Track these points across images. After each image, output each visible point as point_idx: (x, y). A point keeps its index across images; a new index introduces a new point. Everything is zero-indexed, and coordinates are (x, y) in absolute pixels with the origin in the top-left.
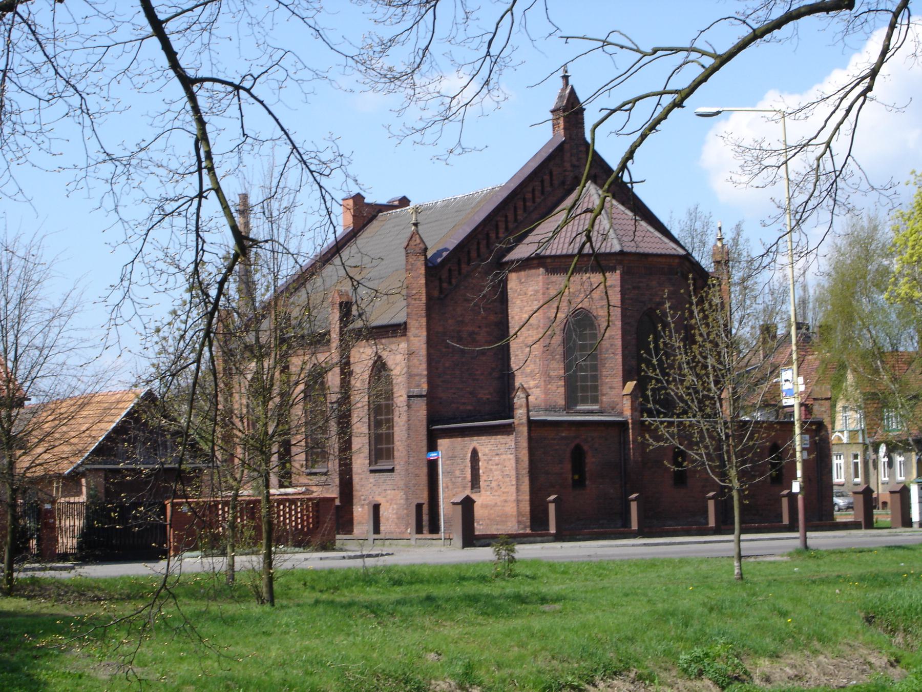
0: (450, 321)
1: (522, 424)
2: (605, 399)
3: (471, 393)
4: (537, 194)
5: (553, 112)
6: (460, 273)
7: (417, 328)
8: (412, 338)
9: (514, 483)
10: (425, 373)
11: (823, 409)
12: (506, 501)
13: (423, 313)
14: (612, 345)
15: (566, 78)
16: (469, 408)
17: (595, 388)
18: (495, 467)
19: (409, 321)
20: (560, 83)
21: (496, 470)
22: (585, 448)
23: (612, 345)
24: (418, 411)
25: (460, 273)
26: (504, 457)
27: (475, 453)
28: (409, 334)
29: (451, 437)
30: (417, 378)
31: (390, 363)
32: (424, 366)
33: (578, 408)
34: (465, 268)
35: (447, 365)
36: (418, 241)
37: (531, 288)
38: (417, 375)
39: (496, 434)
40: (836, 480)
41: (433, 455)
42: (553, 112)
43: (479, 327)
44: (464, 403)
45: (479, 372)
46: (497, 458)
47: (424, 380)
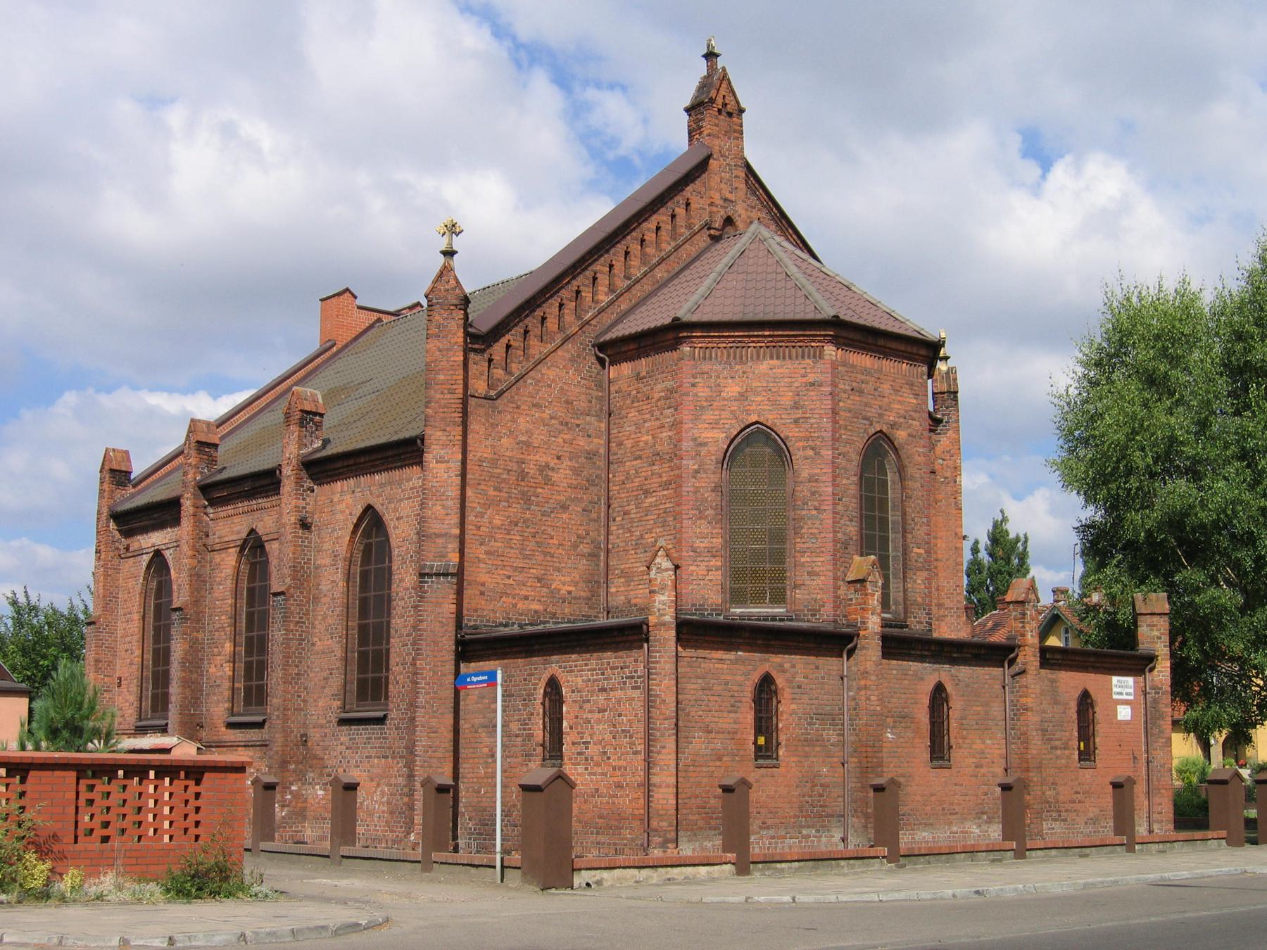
0: (505, 440)
1: (664, 624)
2: (799, 594)
3: (539, 580)
5: (688, 110)
7: (444, 446)
8: (433, 465)
9: (640, 748)
11: (1156, 633)
12: (619, 786)
14: (813, 493)
15: (711, 56)
16: (535, 606)
17: (780, 576)
18: (596, 715)
19: (428, 431)
20: (702, 68)
21: (599, 721)
22: (780, 681)
23: (813, 493)
24: (439, 604)
26: (619, 694)
27: (553, 687)
28: (428, 457)
30: (440, 541)
31: (389, 518)
35: (497, 522)
36: (452, 282)
37: (659, 386)
39: (602, 648)
40: (1115, 679)
41: (870, 650)
42: (688, 110)
43: (559, 458)
44: (526, 598)
46: (602, 697)
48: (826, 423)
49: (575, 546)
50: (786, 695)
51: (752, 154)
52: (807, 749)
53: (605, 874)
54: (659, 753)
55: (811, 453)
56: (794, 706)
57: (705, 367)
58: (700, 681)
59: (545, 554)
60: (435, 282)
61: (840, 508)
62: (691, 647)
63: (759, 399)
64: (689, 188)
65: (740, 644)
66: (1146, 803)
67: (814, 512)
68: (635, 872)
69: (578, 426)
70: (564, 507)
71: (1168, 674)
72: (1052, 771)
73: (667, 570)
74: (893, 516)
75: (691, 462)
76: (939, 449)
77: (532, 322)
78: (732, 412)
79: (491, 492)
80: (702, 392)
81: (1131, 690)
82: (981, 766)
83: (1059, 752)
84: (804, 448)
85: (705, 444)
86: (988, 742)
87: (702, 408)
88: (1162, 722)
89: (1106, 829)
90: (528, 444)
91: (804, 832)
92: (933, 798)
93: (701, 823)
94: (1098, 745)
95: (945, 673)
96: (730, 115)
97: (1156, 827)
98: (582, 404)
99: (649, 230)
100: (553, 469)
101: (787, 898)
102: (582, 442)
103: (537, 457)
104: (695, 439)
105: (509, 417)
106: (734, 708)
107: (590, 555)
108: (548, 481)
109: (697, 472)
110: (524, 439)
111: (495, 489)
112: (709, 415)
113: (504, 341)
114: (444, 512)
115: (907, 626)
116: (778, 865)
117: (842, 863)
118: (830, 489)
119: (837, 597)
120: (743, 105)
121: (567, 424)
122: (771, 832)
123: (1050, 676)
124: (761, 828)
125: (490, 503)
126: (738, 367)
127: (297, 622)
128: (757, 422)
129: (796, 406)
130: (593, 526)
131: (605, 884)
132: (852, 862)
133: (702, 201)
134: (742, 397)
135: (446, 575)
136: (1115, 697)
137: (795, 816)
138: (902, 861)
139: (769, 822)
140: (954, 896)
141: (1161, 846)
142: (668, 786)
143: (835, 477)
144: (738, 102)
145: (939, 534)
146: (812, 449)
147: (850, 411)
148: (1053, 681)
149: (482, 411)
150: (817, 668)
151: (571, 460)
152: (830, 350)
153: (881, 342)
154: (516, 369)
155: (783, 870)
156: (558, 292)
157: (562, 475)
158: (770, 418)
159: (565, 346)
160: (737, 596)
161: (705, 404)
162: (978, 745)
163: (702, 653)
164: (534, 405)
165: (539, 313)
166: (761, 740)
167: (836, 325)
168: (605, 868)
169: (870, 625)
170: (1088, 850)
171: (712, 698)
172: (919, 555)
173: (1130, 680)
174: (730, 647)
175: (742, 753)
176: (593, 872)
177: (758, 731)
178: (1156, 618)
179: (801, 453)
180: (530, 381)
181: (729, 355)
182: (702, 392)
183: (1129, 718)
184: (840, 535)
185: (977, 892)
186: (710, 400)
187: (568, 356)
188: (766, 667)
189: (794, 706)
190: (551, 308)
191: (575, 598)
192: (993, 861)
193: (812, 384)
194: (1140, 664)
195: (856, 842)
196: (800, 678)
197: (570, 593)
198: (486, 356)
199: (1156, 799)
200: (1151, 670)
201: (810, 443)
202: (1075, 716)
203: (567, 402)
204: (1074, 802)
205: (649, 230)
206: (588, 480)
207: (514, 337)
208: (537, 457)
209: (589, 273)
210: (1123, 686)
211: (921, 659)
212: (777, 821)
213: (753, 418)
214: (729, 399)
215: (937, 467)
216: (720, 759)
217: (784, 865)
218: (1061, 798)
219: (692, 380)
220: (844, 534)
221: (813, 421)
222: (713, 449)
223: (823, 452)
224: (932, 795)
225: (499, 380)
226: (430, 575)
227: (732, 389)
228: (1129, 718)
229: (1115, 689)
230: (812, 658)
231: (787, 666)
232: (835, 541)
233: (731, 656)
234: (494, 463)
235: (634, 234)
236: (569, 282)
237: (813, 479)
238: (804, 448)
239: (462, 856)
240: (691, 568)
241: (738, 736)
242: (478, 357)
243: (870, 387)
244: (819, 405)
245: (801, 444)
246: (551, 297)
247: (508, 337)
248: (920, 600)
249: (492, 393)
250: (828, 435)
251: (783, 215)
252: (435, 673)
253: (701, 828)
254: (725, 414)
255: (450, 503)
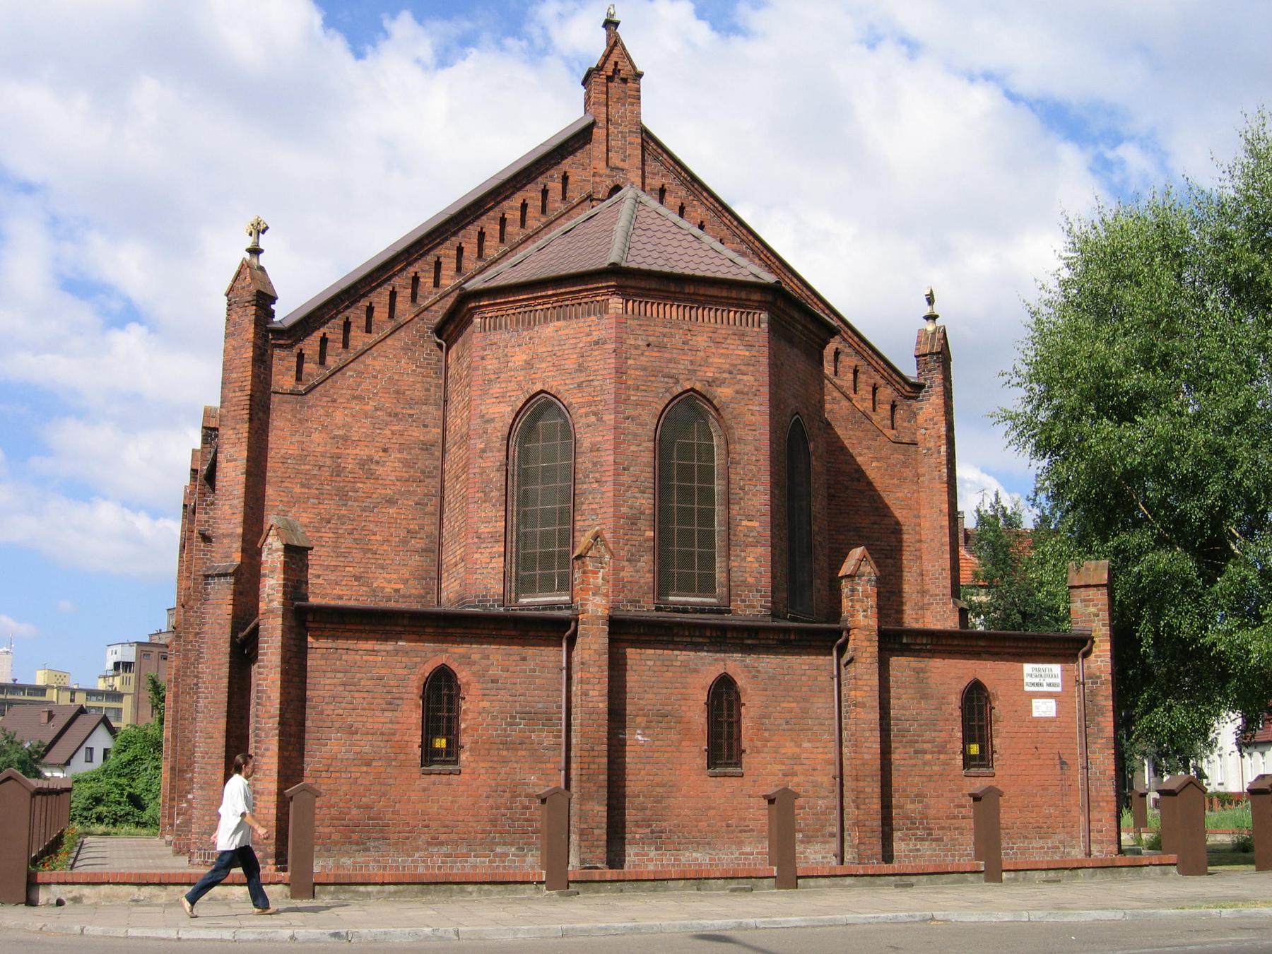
0: (316, 436)
3: (357, 578)
4: (531, 211)
6: (346, 345)
10: (240, 530)
11: (1093, 610)
13: (245, 414)
14: (595, 464)
22: (463, 675)
23: (595, 464)
24: (218, 606)
25: (346, 345)
29: (510, 641)
32: (239, 518)
33: (671, 598)
34: (359, 338)
38: (225, 536)
40: (1028, 668)
43: (385, 450)
45: (378, 537)
47: (237, 545)
48: (610, 385)
49: (405, 542)
50: (472, 691)
51: (652, 117)
52: (505, 753)
53: (87, 891)
54: (263, 755)
55: (593, 419)
56: (486, 704)
57: (494, 337)
58: (339, 675)
59: (365, 551)
60: (235, 280)
61: (625, 478)
62: (372, 639)
63: (544, 365)
64: (568, 161)
65: (401, 633)
66: (1082, 819)
67: (595, 485)
68: (134, 889)
69: (411, 416)
70: (391, 501)
71: (1108, 659)
72: (916, 780)
73: (277, 550)
74: (719, 486)
75: (478, 441)
76: (921, 418)
77: (356, 315)
78: (519, 383)
79: (297, 489)
80: (491, 364)
81: (1059, 680)
82: (795, 774)
83: (928, 757)
84: (587, 415)
85: (492, 420)
86: (806, 745)
87: (490, 381)
88: (1101, 719)
89: (965, 850)
90: (345, 439)
91: (498, 850)
92: (711, 812)
93: (335, 837)
94: (996, 748)
95: (735, 664)
96: (625, 81)
97: (1094, 848)
98: (418, 393)
99: (511, 208)
100: (378, 463)
101: (77, 928)
102: (416, 433)
103: (357, 451)
104: (483, 416)
105: (321, 412)
106: (391, 705)
107: (424, 550)
108: (370, 475)
109: (483, 451)
110: (341, 433)
111: (303, 486)
112: (496, 389)
113: (318, 335)
114: (230, 511)
115: (729, 612)
116: (362, 888)
117: (470, 888)
118: (611, 458)
119: (618, 580)
120: (639, 69)
121: (396, 415)
122: (444, 849)
123: (914, 665)
124: (428, 844)
125: (294, 501)
126: (525, 333)
127: (197, 634)
128: (542, 391)
129: (581, 368)
130: (428, 520)
131: (85, 901)
132: (486, 887)
133: (584, 173)
134: (529, 365)
135: (225, 575)
136: (1027, 688)
137: (484, 831)
138: (573, 887)
139: (442, 837)
140: (292, 938)
141: (1052, 874)
142: (270, 794)
143: (617, 446)
144: (634, 67)
145: (923, 512)
146: (595, 414)
147: (645, 369)
148: (917, 671)
149: (287, 407)
150: (524, 659)
151: (401, 451)
152: (616, 303)
153: (690, 289)
154: (331, 361)
155: (368, 894)
156: (389, 279)
157: (390, 469)
158: (554, 385)
159: (396, 335)
160: (526, 586)
161: (493, 377)
162: (789, 748)
163: (341, 643)
164: (354, 398)
165: (364, 303)
166: (974, 749)
167: (615, 271)
168: (88, 884)
169: (590, 607)
170: (913, 879)
171: (356, 695)
172: (751, 529)
173: (1056, 668)
174: (385, 637)
175: (402, 757)
176: (69, 888)
177: (967, 739)
178: (1092, 592)
179: (583, 420)
180: (349, 373)
181: (518, 322)
182: (491, 364)
183: (1053, 714)
184: (623, 510)
185: (336, 935)
186: (498, 372)
187: (399, 344)
188: (442, 659)
189: (486, 704)
190: (380, 298)
191: (404, 596)
192: (733, 890)
193: (596, 343)
194: (1069, 648)
195: (966, 863)
196: (494, 671)
197: (397, 591)
198: (296, 350)
199: (1095, 815)
200: (1086, 655)
201: (593, 408)
202: (958, 713)
203: (398, 392)
204: (955, 817)
205: (511, 208)
206: (423, 472)
207: (332, 329)
208: (357, 451)
209: (431, 258)
210: (1042, 680)
211: (696, 647)
212: (454, 836)
213: (538, 387)
214: (516, 369)
215: (919, 438)
216: (368, 764)
217: (370, 888)
218: (932, 812)
219: (481, 353)
220: (631, 507)
221: (596, 383)
222: (498, 425)
223: (606, 417)
224: (710, 808)
225: (311, 375)
226: (212, 576)
227: (519, 358)
228: (1053, 714)
229: (1027, 679)
230: (516, 649)
231: (475, 657)
232: (617, 516)
233: (389, 646)
234: (302, 459)
235: (491, 213)
236: (402, 270)
237: (595, 448)
238: (587, 415)
239: (895, 866)
240: (476, 556)
241: (397, 738)
242: (284, 353)
243: (677, 340)
244: (603, 364)
245: (583, 410)
246: (379, 285)
247: (322, 330)
248: (751, 580)
249: (302, 388)
250: (611, 398)
251: (694, 179)
252: (213, 677)
253: (336, 843)
254: (513, 386)
255: (236, 502)
